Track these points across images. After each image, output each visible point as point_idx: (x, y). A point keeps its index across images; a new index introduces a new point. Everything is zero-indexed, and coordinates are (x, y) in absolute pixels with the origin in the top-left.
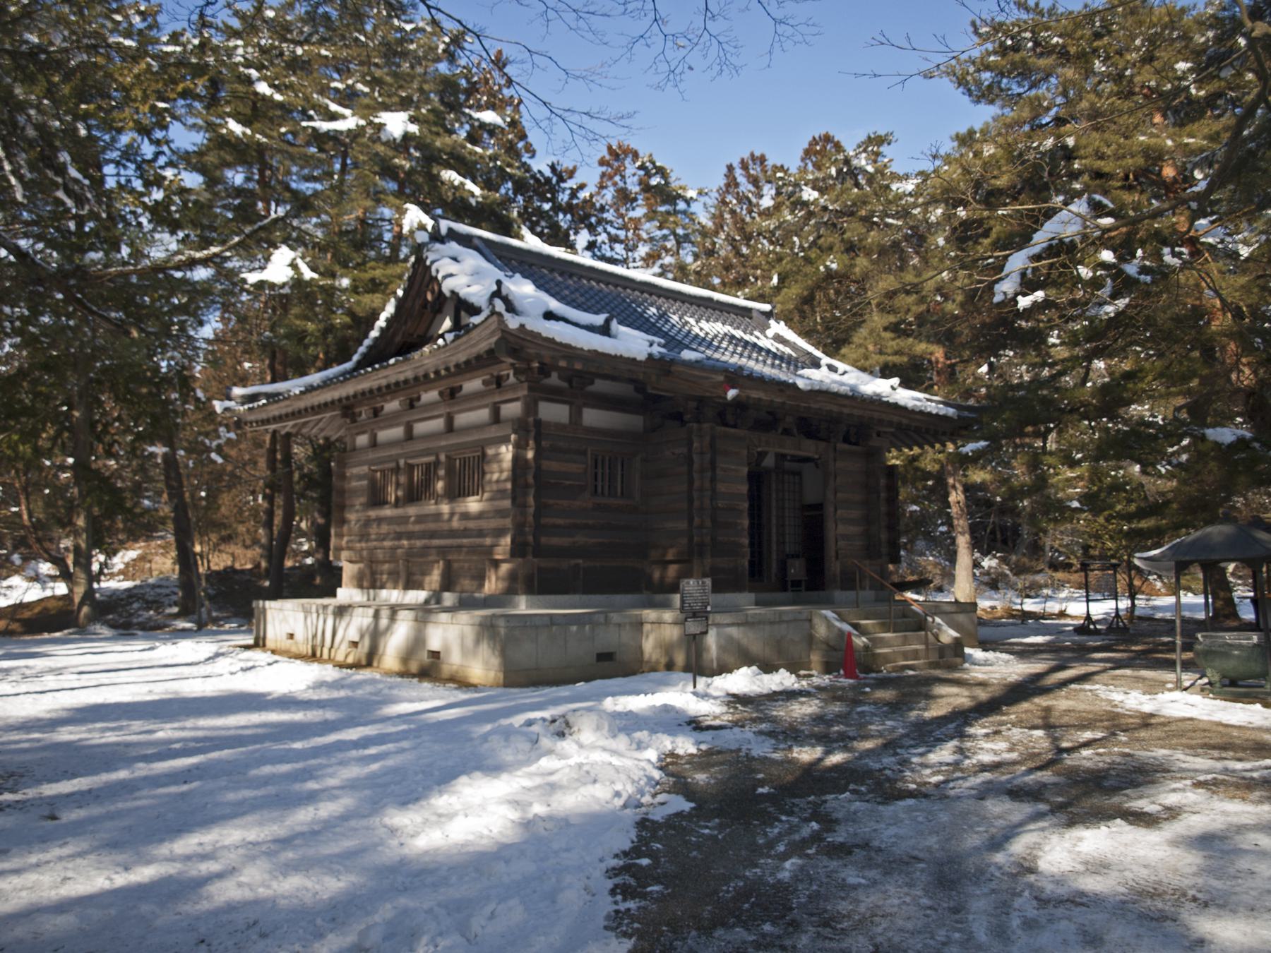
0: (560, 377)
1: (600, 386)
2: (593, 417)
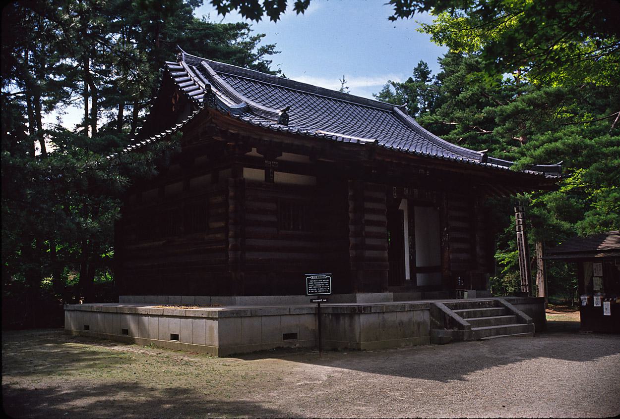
0: (258, 151)
1: (286, 156)
2: (280, 177)
